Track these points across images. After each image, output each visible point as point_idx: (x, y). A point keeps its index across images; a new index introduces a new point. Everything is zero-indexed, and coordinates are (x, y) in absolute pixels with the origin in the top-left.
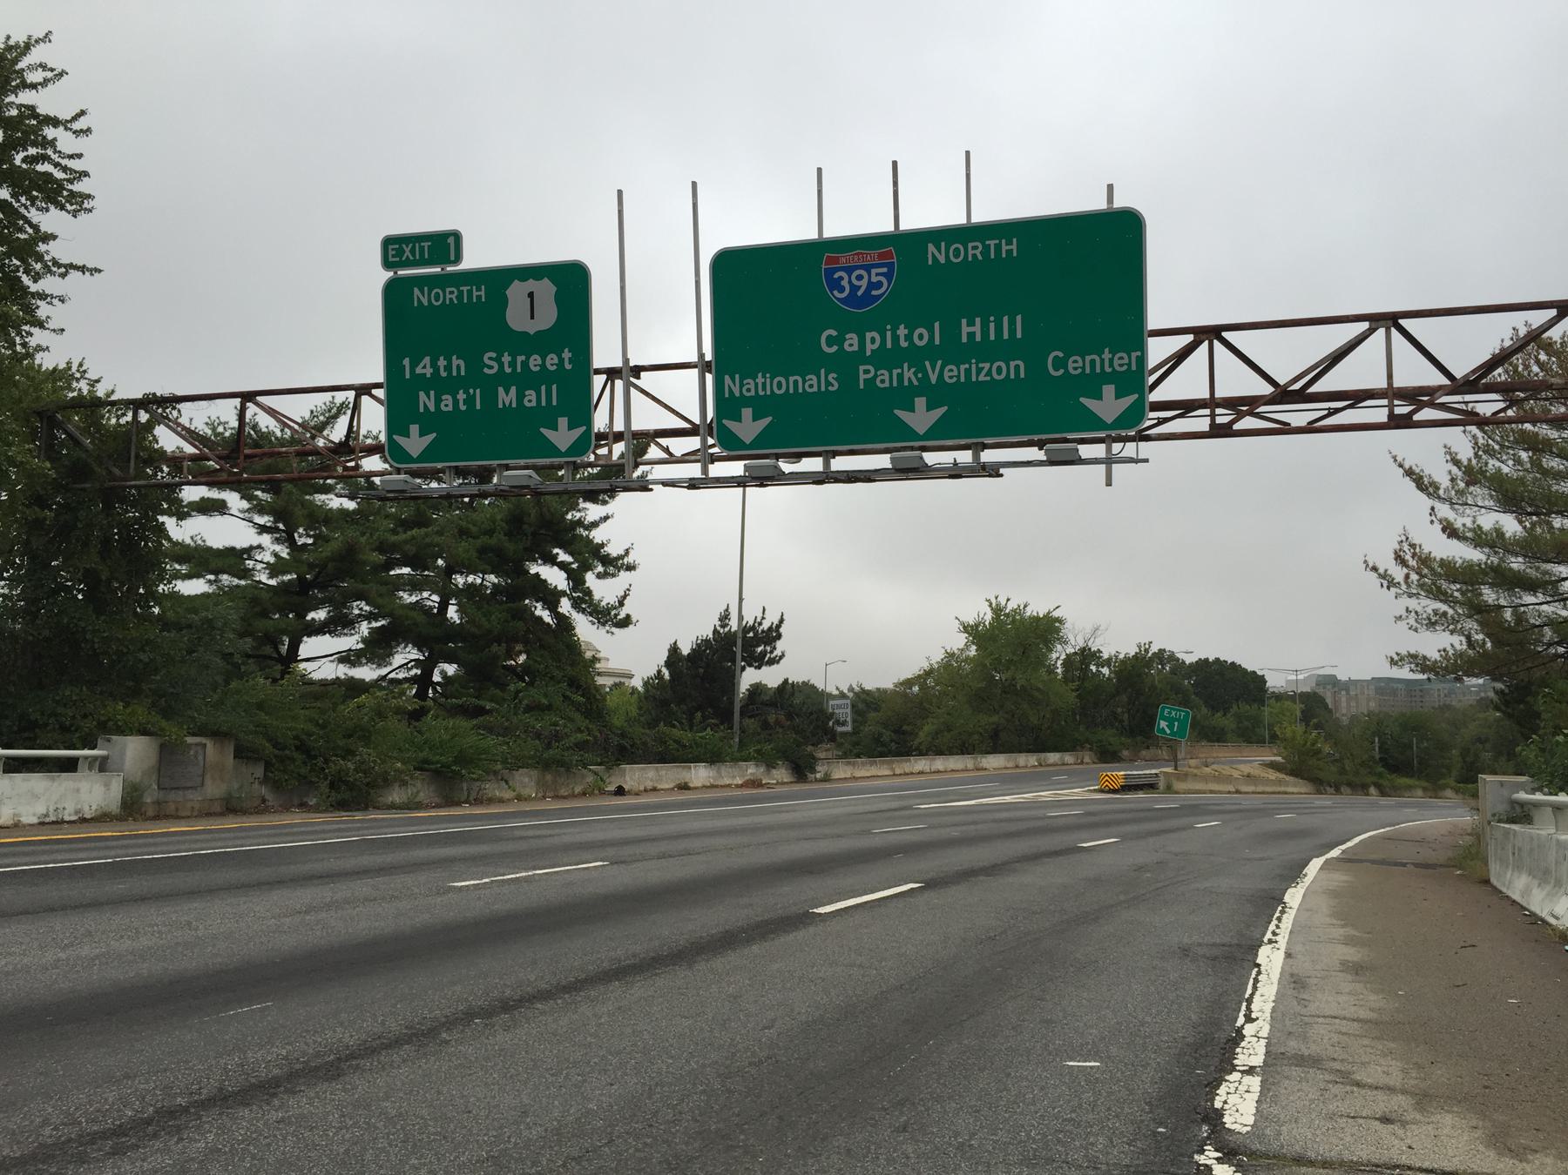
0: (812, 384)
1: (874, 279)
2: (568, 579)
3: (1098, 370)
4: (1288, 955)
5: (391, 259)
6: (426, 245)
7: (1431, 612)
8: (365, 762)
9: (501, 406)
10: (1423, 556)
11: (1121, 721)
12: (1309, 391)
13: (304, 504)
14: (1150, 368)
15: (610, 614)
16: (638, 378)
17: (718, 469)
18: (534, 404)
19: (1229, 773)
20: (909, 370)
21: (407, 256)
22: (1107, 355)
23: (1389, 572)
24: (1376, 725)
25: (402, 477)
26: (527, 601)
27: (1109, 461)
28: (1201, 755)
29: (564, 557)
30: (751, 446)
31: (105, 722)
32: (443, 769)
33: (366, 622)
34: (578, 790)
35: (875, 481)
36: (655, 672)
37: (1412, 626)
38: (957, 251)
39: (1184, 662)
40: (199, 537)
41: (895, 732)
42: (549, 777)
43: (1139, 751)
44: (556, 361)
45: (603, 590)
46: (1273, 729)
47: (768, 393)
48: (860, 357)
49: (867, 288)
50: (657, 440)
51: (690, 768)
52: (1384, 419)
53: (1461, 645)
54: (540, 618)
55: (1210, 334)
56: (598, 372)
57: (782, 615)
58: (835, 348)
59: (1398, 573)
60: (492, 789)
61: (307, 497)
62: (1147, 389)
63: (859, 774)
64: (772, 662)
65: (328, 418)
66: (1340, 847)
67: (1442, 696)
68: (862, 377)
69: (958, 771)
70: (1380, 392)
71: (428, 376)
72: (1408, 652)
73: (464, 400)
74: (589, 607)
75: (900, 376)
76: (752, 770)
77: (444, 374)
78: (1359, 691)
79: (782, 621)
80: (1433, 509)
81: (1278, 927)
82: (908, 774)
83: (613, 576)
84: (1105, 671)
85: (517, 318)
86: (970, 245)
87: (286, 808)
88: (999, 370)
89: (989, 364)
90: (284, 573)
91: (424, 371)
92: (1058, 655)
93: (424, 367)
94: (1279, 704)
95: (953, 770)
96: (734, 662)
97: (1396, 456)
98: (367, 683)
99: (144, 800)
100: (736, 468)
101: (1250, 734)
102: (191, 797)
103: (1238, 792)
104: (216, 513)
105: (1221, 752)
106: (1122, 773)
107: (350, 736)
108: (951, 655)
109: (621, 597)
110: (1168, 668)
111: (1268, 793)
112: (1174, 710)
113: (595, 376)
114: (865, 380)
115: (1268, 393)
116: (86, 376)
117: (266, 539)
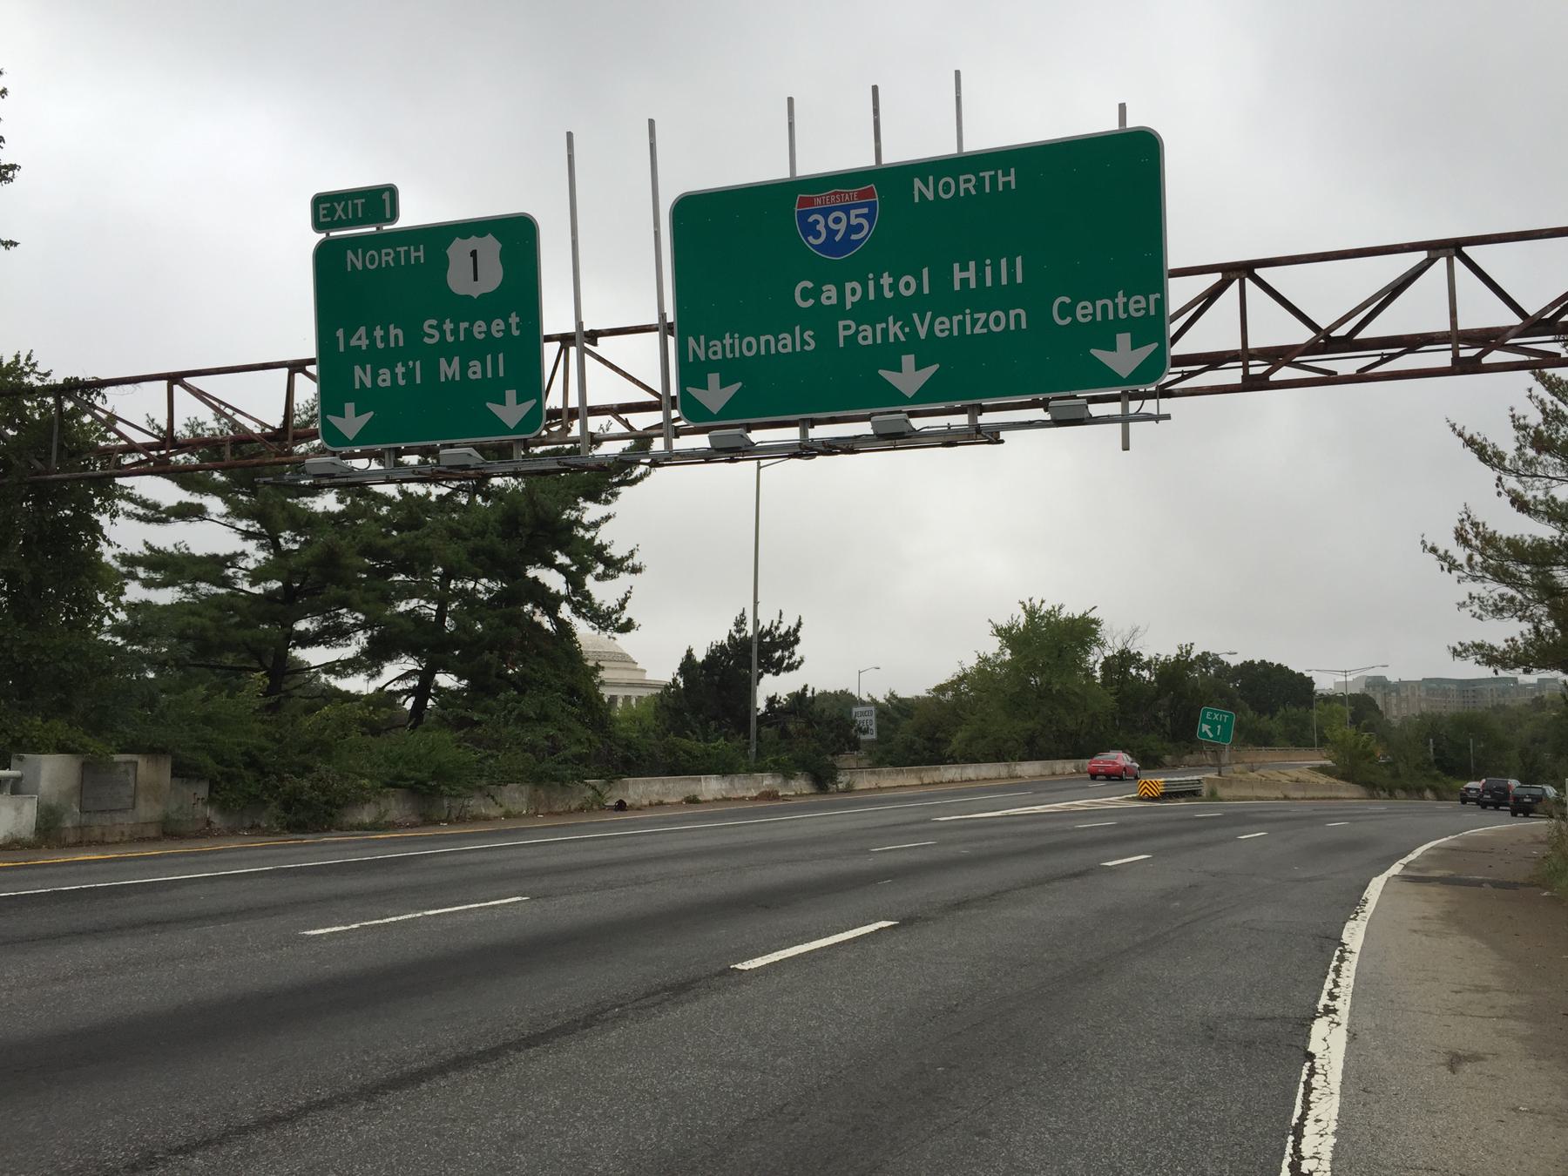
0: (786, 343)
1: (854, 221)
2: (567, 583)
3: (1111, 317)
4: (1353, 1036)
5: (322, 220)
6: (359, 202)
7: (1497, 597)
8: (323, 778)
9: (443, 379)
10: (1488, 536)
11: (1163, 726)
12: (1358, 337)
13: (284, 506)
14: (1170, 314)
15: (610, 618)
16: (595, 344)
17: (683, 443)
18: (479, 376)
19: (1276, 779)
20: (894, 324)
21: (340, 216)
22: (1121, 299)
23: (1449, 553)
24: (1430, 727)
25: (329, 459)
26: (528, 607)
27: (1125, 419)
28: (1246, 760)
29: (562, 559)
30: (720, 416)
31: (20, 740)
32: (418, 786)
33: (362, 632)
34: (575, 804)
35: (858, 452)
36: (671, 681)
37: (1475, 613)
38: (947, 184)
39: (1228, 665)
40: (183, 544)
41: (929, 739)
42: (541, 793)
43: (1182, 756)
44: (502, 327)
45: (603, 592)
46: (1323, 733)
47: (737, 355)
48: (839, 311)
49: (845, 232)
50: (620, 415)
51: (700, 780)
52: (1448, 363)
53: (1530, 634)
54: (539, 624)
55: (1241, 271)
56: (549, 339)
57: (800, 619)
58: (811, 302)
59: (1460, 554)
60: (477, 805)
61: (289, 500)
62: (1168, 342)
63: (885, 783)
64: (790, 668)
65: (311, 417)
66: (1401, 861)
67: (1495, 695)
68: (842, 334)
69: (990, 779)
70: (1440, 336)
71: (364, 348)
72: (1473, 642)
73: (403, 373)
74: (588, 612)
75: (885, 332)
76: (768, 781)
77: (380, 345)
78: (1409, 693)
79: (799, 624)
80: (1499, 479)
81: (1336, 985)
82: (937, 783)
83: (613, 577)
84: (1145, 673)
85: (459, 280)
86: (962, 178)
87: (233, 832)
88: (997, 321)
89: (985, 314)
90: (266, 580)
91: (359, 343)
92: (1096, 658)
93: (360, 339)
94: (1328, 706)
95: (985, 779)
96: (750, 667)
97: (1455, 424)
98: (353, 694)
99: (63, 825)
100: (702, 441)
101: (1299, 738)
102: (121, 820)
103: (1286, 798)
104: (195, 519)
105: (1265, 755)
106: (1162, 780)
107: (308, 751)
108: (985, 660)
109: (622, 599)
110: (1212, 671)
111: (1318, 799)
112: (1217, 712)
113: (545, 344)
114: (845, 337)
115: (1304, 342)
116: (37, 369)
117: (251, 546)
